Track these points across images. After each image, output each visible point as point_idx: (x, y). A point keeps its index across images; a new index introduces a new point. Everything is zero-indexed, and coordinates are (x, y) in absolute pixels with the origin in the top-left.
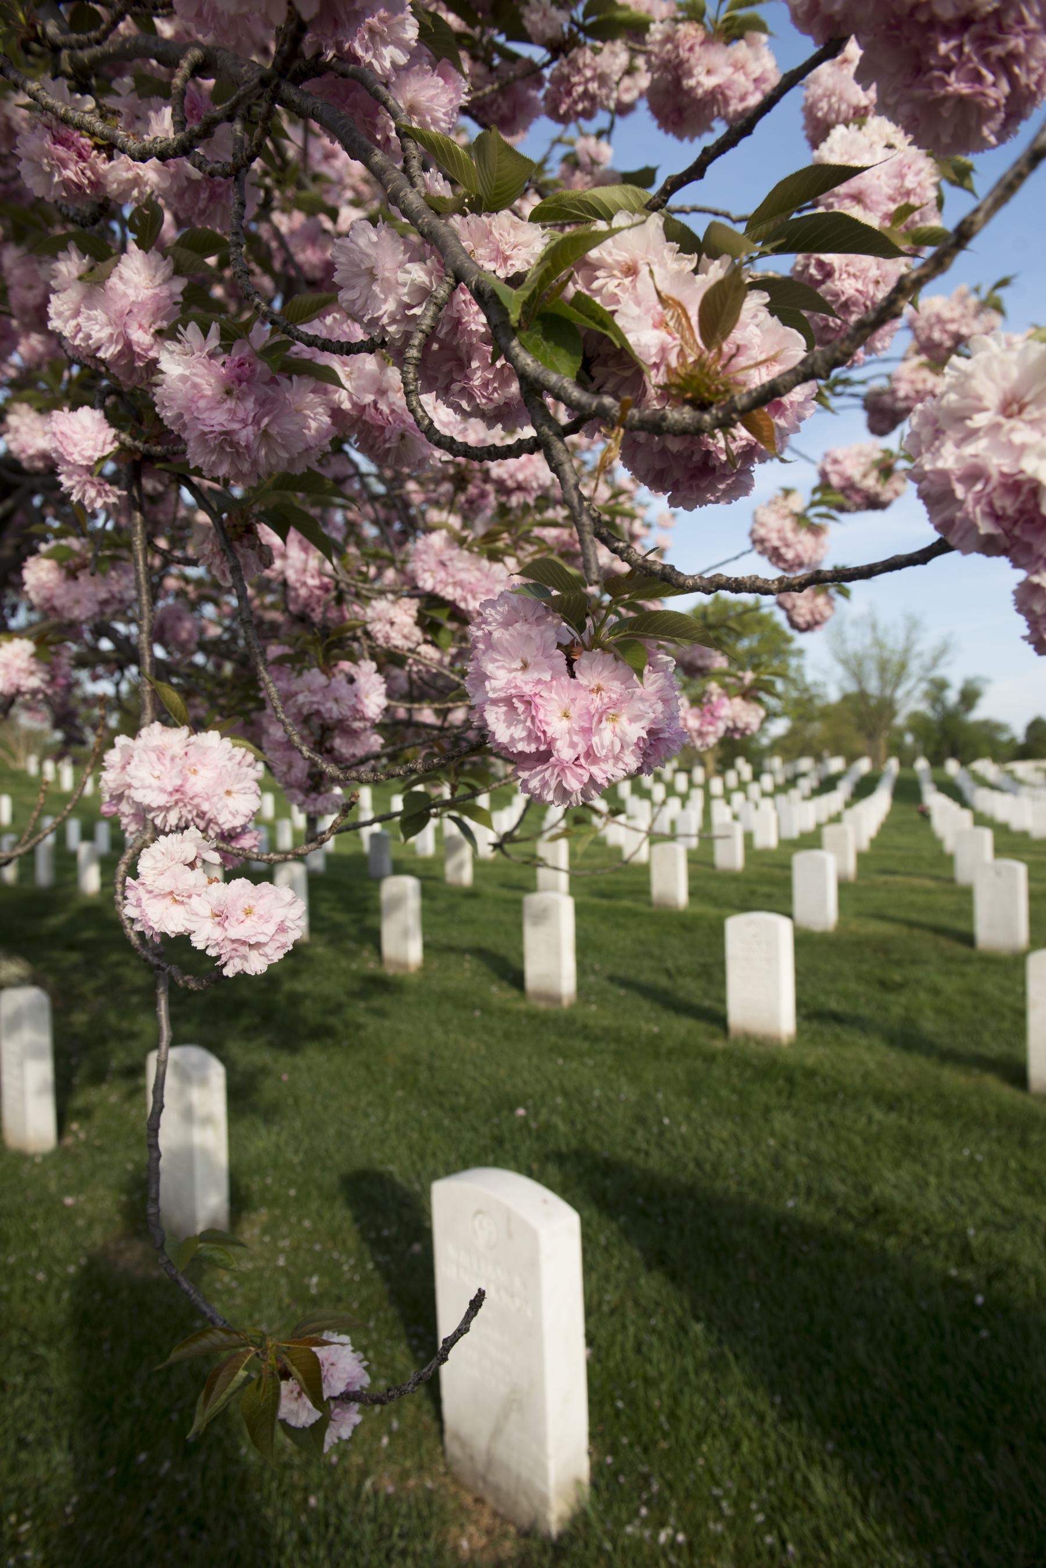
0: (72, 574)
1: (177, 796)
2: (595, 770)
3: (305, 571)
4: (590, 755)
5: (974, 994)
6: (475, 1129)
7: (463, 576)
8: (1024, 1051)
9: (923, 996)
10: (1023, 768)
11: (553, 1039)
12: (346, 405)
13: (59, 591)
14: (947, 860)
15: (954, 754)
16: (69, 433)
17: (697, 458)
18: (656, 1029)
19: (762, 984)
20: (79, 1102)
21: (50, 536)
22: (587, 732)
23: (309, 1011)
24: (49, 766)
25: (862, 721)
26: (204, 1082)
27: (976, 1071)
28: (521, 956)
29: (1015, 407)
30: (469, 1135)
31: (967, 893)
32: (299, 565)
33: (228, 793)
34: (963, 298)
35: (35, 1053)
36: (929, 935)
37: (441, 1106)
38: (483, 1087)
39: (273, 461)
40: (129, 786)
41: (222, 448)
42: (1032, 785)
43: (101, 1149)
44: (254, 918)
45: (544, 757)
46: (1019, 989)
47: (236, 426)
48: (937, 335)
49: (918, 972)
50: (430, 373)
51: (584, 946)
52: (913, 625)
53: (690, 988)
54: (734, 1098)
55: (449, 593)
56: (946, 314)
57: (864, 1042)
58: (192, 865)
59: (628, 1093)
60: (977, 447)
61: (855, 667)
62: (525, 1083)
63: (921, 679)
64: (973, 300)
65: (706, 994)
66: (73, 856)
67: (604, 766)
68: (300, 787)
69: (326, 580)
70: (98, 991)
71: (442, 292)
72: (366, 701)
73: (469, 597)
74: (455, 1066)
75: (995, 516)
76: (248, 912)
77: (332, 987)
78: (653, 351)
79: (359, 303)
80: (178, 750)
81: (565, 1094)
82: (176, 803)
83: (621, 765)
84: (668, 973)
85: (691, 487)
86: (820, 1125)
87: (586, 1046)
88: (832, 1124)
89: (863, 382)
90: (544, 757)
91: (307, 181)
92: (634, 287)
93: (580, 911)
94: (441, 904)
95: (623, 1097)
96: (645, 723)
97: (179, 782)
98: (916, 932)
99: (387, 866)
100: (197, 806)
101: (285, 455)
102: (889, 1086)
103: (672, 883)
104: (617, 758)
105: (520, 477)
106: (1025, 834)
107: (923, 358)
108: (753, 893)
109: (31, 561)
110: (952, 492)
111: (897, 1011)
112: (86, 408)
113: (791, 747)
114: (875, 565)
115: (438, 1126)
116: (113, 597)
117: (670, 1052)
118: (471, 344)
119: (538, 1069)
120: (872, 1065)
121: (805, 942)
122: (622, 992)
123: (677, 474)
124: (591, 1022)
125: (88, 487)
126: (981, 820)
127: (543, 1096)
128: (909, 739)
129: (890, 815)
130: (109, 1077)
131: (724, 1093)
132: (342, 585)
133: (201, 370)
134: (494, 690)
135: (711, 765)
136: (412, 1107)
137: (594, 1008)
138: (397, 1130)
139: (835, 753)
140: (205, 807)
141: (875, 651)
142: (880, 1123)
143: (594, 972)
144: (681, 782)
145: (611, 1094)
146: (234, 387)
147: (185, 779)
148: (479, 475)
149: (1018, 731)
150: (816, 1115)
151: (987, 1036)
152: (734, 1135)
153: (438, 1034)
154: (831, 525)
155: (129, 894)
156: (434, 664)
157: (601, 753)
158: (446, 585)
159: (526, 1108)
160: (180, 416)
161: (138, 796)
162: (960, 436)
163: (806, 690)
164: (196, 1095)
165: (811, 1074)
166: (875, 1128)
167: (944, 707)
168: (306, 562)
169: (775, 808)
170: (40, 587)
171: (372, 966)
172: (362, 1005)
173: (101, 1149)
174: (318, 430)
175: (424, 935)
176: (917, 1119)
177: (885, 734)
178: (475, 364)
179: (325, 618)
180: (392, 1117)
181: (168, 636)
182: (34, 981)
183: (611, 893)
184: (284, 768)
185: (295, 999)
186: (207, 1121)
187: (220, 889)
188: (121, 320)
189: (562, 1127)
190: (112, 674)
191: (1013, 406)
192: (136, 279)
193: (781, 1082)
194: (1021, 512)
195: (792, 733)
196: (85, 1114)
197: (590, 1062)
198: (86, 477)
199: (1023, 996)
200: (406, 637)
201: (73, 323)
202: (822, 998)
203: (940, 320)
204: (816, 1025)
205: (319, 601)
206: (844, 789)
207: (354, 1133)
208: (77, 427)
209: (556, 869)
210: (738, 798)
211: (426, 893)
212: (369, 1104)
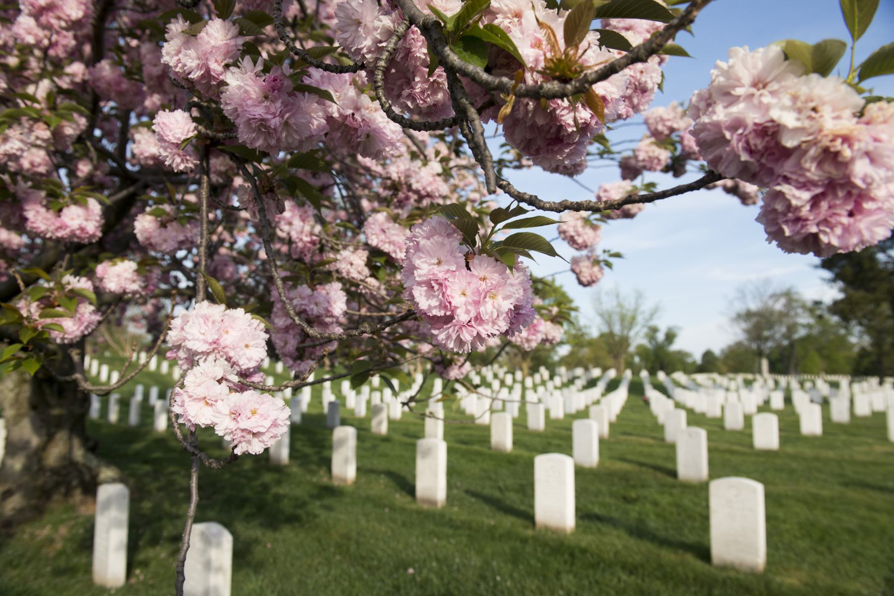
0: (163, 225)
1: (215, 346)
2: (480, 329)
3: (302, 232)
4: (478, 319)
5: (678, 505)
6: (383, 581)
7: (395, 238)
8: (709, 540)
9: (649, 506)
10: (701, 378)
11: (432, 527)
12: (336, 115)
13: (155, 234)
14: (661, 428)
15: (662, 368)
16: (168, 123)
17: (553, 130)
18: (492, 522)
19: (555, 498)
20: (141, 556)
21: (150, 202)
22: (477, 303)
23: (286, 506)
24: (143, 356)
25: (611, 349)
26: (219, 545)
27: (680, 552)
28: (414, 476)
29: (761, 85)
30: (379, 584)
31: (672, 447)
32: (299, 229)
33: (247, 346)
34: (674, 108)
35: (117, 524)
36: (651, 471)
37: (363, 566)
38: (389, 556)
39: (290, 141)
40: (185, 339)
41: (260, 130)
42: (707, 387)
43: (152, 586)
44: (257, 416)
45: (448, 319)
46: (704, 503)
47: (269, 117)
48: (660, 127)
49: (645, 492)
50: (389, 86)
51: (452, 472)
52: (639, 296)
53: (513, 498)
54: (539, 565)
55: (386, 248)
56: (665, 116)
57: (615, 533)
58: (219, 381)
59: (476, 560)
60: (738, 109)
61: (607, 318)
62: (414, 553)
63: (644, 326)
64: (680, 110)
65: (522, 502)
66: (152, 409)
67: (486, 327)
68: (291, 356)
69: (314, 238)
70: (160, 489)
71: (401, 29)
72: (334, 306)
73: (398, 250)
74: (372, 541)
75: (750, 151)
76: (254, 413)
77: (300, 492)
78: (531, 59)
79: (351, 39)
80: (218, 318)
81: (438, 560)
82: (214, 350)
83: (496, 327)
84: (500, 489)
85: (548, 151)
86: (590, 583)
87: (451, 531)
88: (597, 582)
89: (619, 153)
90: (448, 319)
91: (317, 26)
92: (521, 24)
93: (450, 451)
94: (368, 444)
95: (473, 563)
96: (512, 300)
97: (216, 337)
98: (644, 469)
99: (338, 421)
100: (226, 353)
101: (297, 137)
102: (630, 560)
103: (503, 437)
104: (494, 323)
105: (429, 189)
106: (703, 415)
107: (653, 139)
108: (549, 444)
109: (140, 217)
110: (724, 137)
111: (634, 515)
112: (180, 110)
113: (571, 362)
114: (667, 191)
115: (361, 578)
116: (187, 239)
117: (501, 536)
118: (416, 67)
119: (422, 545)
120: (620, 547)
121: (580, 473)
122: (473, 500)
123: (540, 142)
124: (454, 517)
125: (176, 157)
126: (678, 405)
127: (424, 561)
128: (637, 359)
129: (628, 401)
130: (162, 542)
131: (533, 562)
132: (324, 241)
133: (250, 82)
134: (420, 276)
135: (526, 371)
136: (345, 566)
137: (456, 509)
138: (335, 580)
139: (596, 365)
140: (231, 354)
141: (618, 310)
142: (625, 582)
143: (457, 487)
144: (509, 379)
145: (466, 562)
146: (270, 93)
147: (221, 336)
148: (405, 186)
149: (698, 357)
150: (587, 576)
151: (686, 531)
152: (538, 588)
153: (363, 522)
154: (602, 225)
155: (178, 398)
156: (375, 289)
157: (485, 317)
158: (385, 243)
159: (414, 568)
160: (236, 110)
161: (190, 345)
162: (725, 104)
163: (580, 329)
164: (214, 553)
165: (584, 551)
166: (622, 585)
167: (656, 343)
168: (303, 227)
169: (562, 395)
170: (144, 230)
171: (325, 480)
172: (318, 503)
173: (152, 586)
174: (318, 126)
175: (357, 462)
176: (647, 580)
177: (624, 356)
178: (417, 79)
179: (312, 260)
180: (333, 572)
181: (219, 275)
182: (121, 480)
183: (467, 440)
184: (282, 344)
185: (278, 498)
186: (219, 569)
187: (235, 396)
188: (204, 58)
189: (436, 581)
190: (185, 302)
191: (759, 83)
192: (216, 35)
193: (567, 556)
194: (766, 148)
195: (572, 354)
196: (145, 564)
197: (453, 541)
198: (175, 151)
199: (707, 507)
200: (359, 273)
201: (176, 58)
202: (590, 506)
203: (662, 120)
204: (586, 522)
205: (309, 250)
206: (601, 386)
207: (309, 581)
208: (173, 121)
209: (438, 419)
210: (541, 389)
211: (360, 438)
212: (319, 564)
